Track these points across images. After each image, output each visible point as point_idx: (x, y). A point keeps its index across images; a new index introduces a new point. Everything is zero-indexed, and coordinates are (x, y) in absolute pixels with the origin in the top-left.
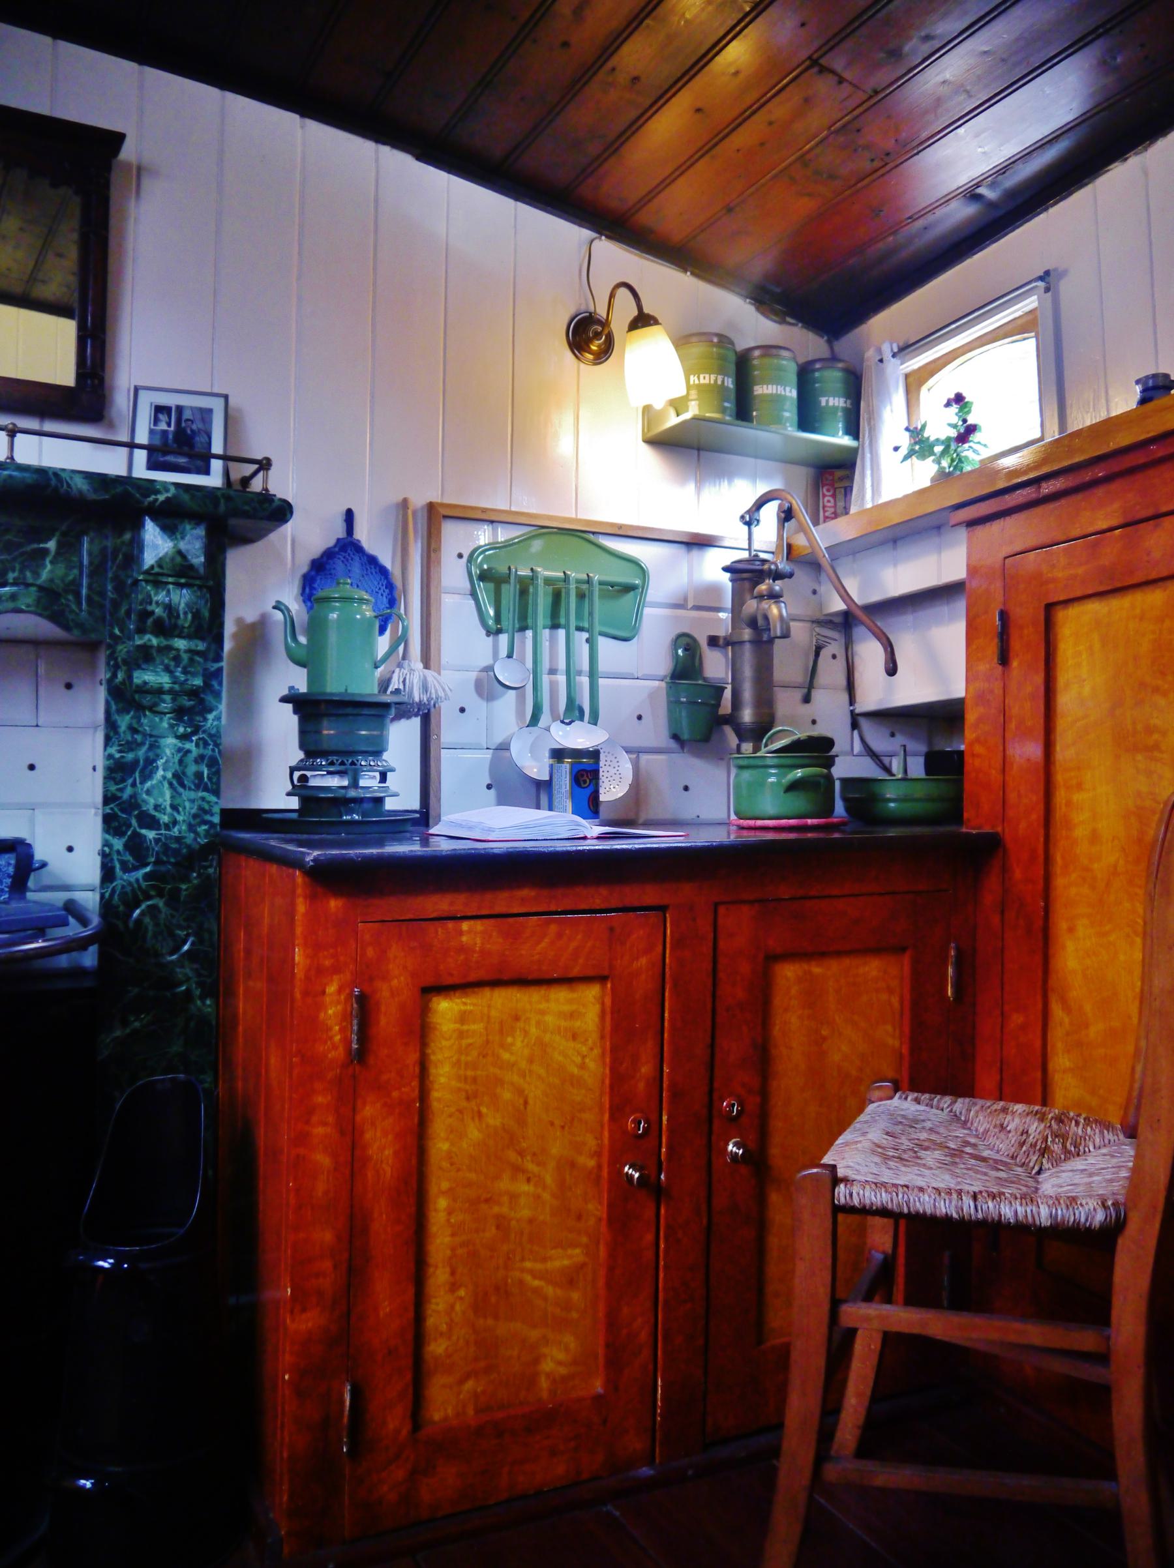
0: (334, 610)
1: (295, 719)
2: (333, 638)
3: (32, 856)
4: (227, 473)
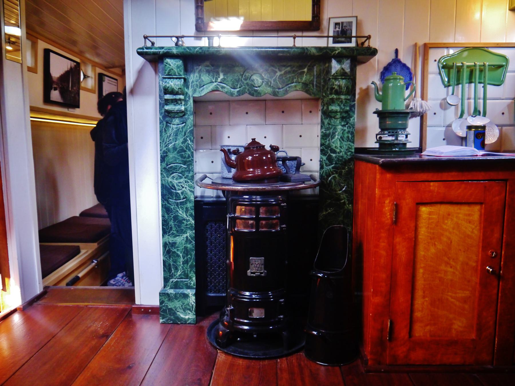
0: (391, 82)
1: (378, 119)
2: (390, 92)
3: (301, 161)
4: (357, 42)
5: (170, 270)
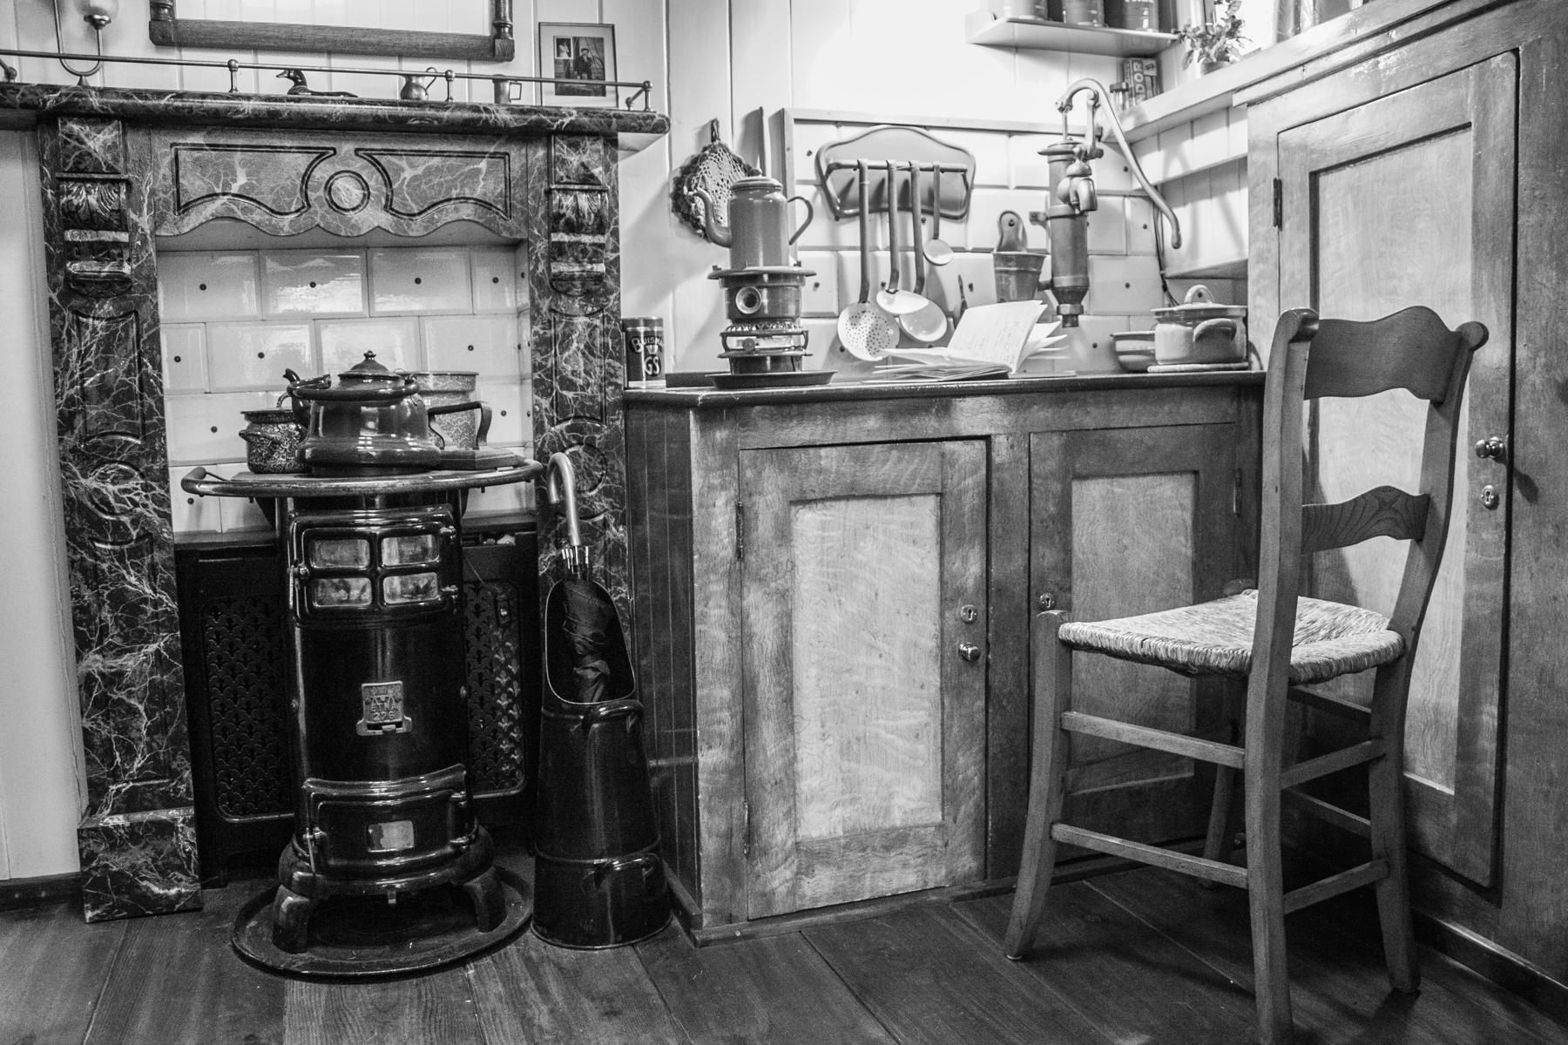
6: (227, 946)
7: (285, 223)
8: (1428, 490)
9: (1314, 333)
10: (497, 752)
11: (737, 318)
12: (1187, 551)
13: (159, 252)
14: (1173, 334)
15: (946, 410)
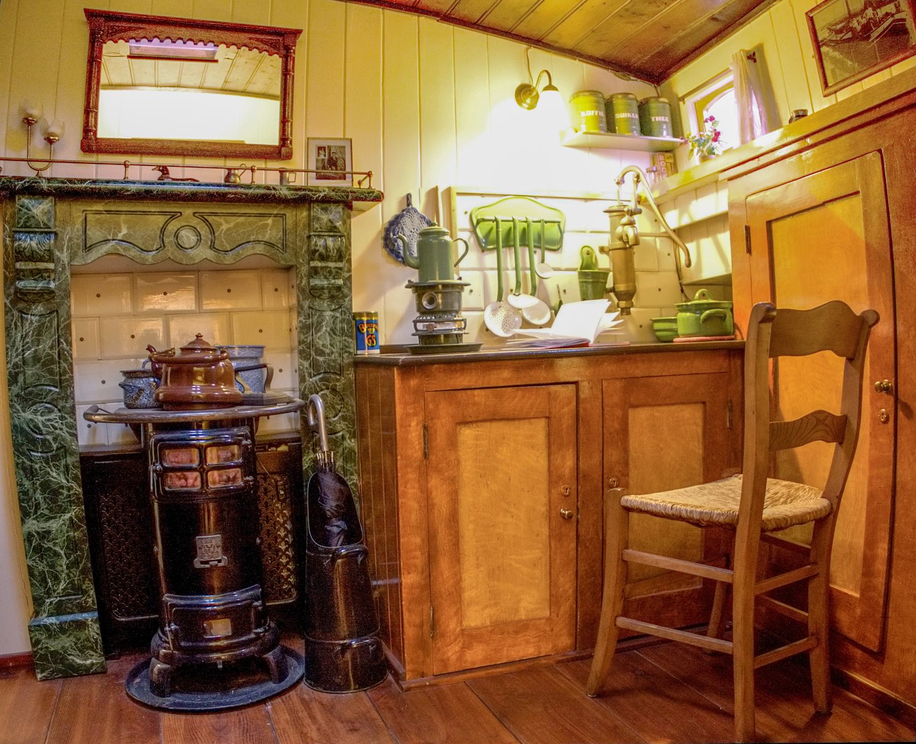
5: (44, 581)
6: (124, 694)
7: (149, 257)
8: (846, 413)
9: (774, 318)
10: (280, 577)
11: (423, 312)
12: (700, 451)
13: (72, 275)
14: (688, 318)
15: (551, 366)
